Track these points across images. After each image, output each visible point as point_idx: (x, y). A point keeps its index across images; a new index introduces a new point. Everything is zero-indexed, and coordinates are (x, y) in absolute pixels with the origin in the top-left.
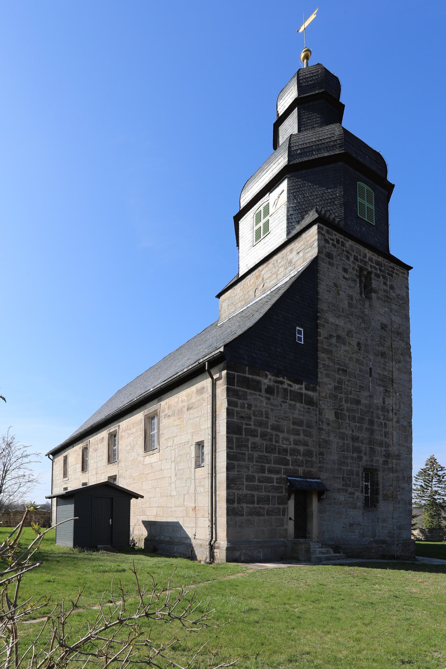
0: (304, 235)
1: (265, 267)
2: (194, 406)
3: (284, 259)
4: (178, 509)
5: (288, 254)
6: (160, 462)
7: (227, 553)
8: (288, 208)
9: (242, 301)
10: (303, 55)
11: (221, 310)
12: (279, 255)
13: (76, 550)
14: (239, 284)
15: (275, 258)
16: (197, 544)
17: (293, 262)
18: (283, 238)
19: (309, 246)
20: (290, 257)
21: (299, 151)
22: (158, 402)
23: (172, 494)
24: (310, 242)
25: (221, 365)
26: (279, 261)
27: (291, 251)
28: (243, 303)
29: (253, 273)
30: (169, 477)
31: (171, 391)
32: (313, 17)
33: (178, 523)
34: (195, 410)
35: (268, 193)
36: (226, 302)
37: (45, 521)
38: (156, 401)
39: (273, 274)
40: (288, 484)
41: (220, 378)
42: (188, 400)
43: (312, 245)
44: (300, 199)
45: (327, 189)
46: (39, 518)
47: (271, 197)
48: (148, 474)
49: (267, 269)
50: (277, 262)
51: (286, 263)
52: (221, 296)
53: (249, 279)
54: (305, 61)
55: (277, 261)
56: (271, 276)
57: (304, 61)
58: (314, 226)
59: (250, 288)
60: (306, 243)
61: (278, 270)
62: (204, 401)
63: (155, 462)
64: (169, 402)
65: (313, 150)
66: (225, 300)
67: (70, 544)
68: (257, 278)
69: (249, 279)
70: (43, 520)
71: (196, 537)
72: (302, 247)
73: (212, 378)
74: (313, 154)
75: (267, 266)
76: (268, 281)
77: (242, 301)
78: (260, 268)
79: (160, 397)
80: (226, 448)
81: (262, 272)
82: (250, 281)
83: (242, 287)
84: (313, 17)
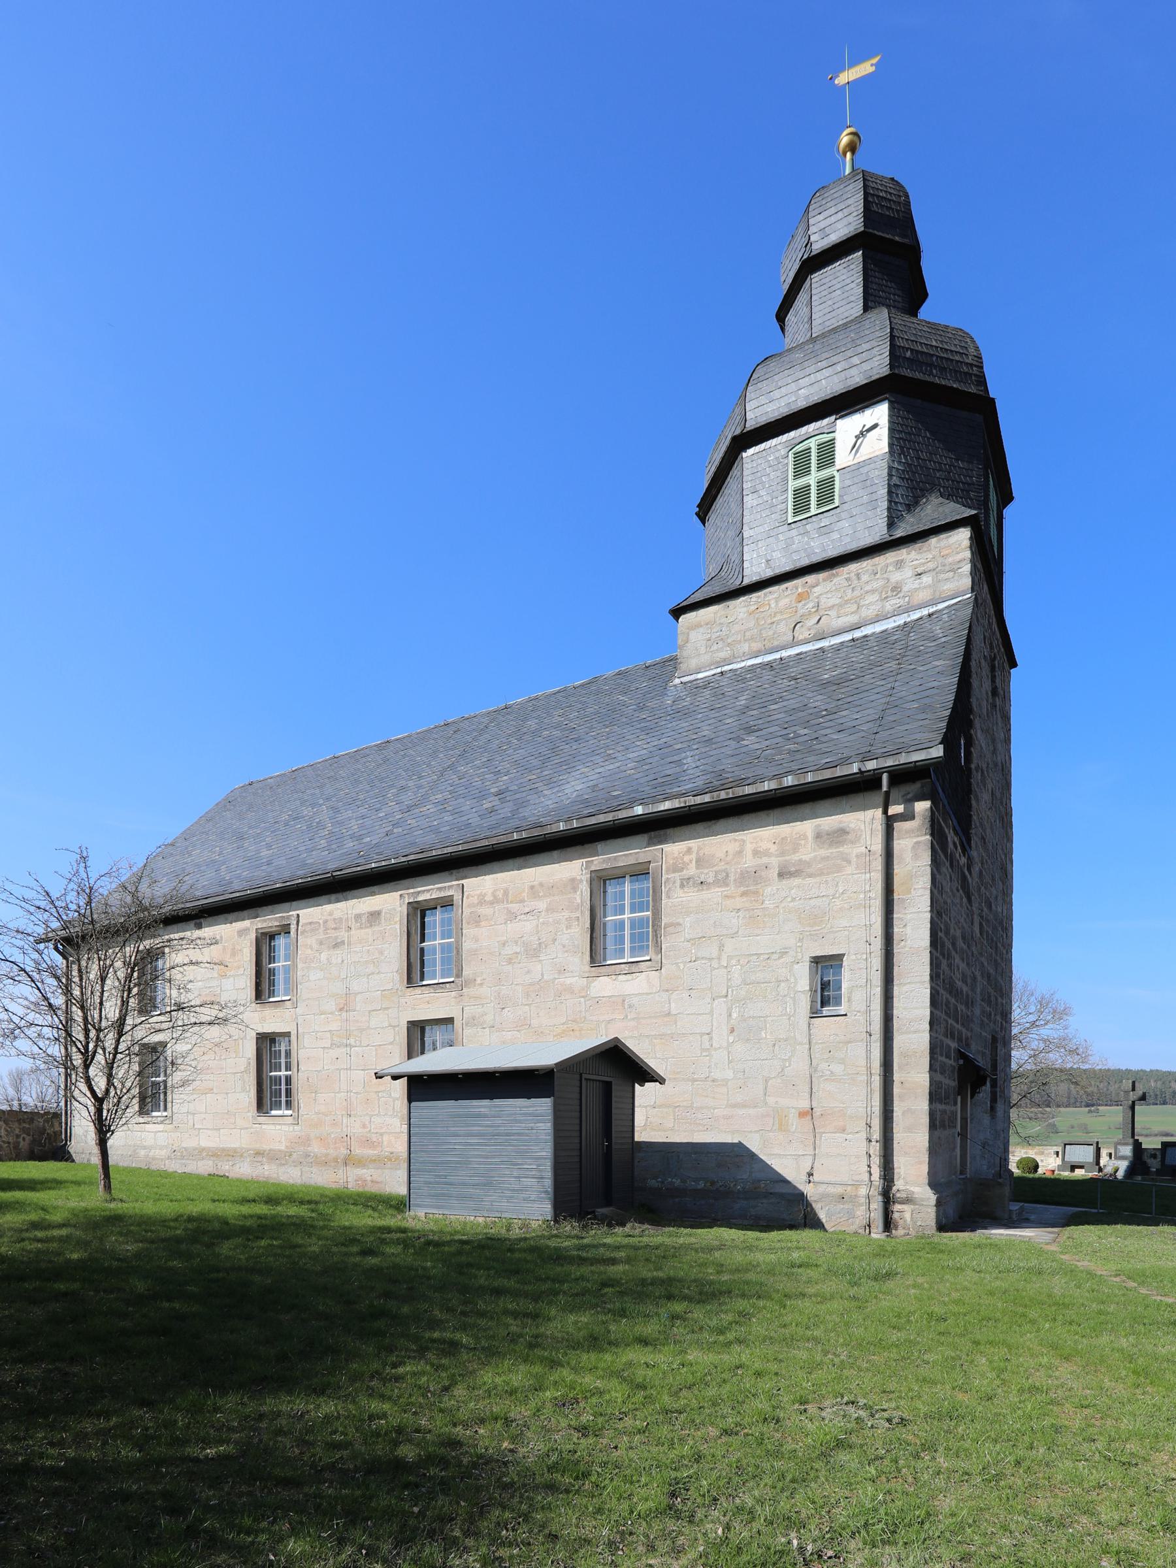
0: (933, 541)
1: (824, 580)
2: (810, 870)
3: (878, 576)
4: (741, 1112)
5: (890, 568)
6: (665, 995)
7: (937, 1212)
8: (890, 468)
9: (752, 639)
10: (845, 140)
11: (683, 646)
12: (865, 565)
13: (569, 1227)
14: (742, 599)
15: (853, 567)
16: (824, 1196)
17: (905, 589)
18: (875, 530)
19: (947, 568)
20: (896, 577)
21: (908, 354)
22: (649, 845)
23: (717, 1074)
24: (950, 560)
25: (915, 787)
26: (865, 578)
27: (899, 565)
28: (756, 646)
29: (790, 584)
30: (702, 1034)
31: (710, 823)
32: (866, 68)
33: (740, 1145)
34: (809, 880)
35: (833, 417)
36: (701, 630)
37: (34, 1141)
38: (643, 838)
39: (847, 602)
40: (961, 1062)
41: (908, 816)
42: (782, 854)
43: (956, 567)
44: (912, 458)
45: (957, 460)
46: (17, 1131)
47: (846, 428)
48: (609, 1022)
49: (829, 585)
50: (859, 579)
51: (884, 587)
52: (684, 613)
53: (775, 595)
54: (849, 155)
55: (858, 576)
56: (840, 606)
57: (845, 155)
58: (962, 530)
59: (778, 617)
60: (940, 560)
61: (862, 597)
62: (849, 862)
63: (639, 994)
64: (699, 849)
65: (931, 365)
66: (699, 626)
67: (546, 1209)
68: (801, 598)
69: (775, 595)
70: (28, 1138)
71: (816, 1178)
72: (931, 565)
73: (885, 812)
74: (931, 373)
75: (829, 579)
76: (833, 613)
77: (752, 639)
78: (810, 579)
79: (662, 832)
80: (928, 978)
81: (816, 589)
82: (777, 600)
83: (753, 608)
84: (866, 68)
